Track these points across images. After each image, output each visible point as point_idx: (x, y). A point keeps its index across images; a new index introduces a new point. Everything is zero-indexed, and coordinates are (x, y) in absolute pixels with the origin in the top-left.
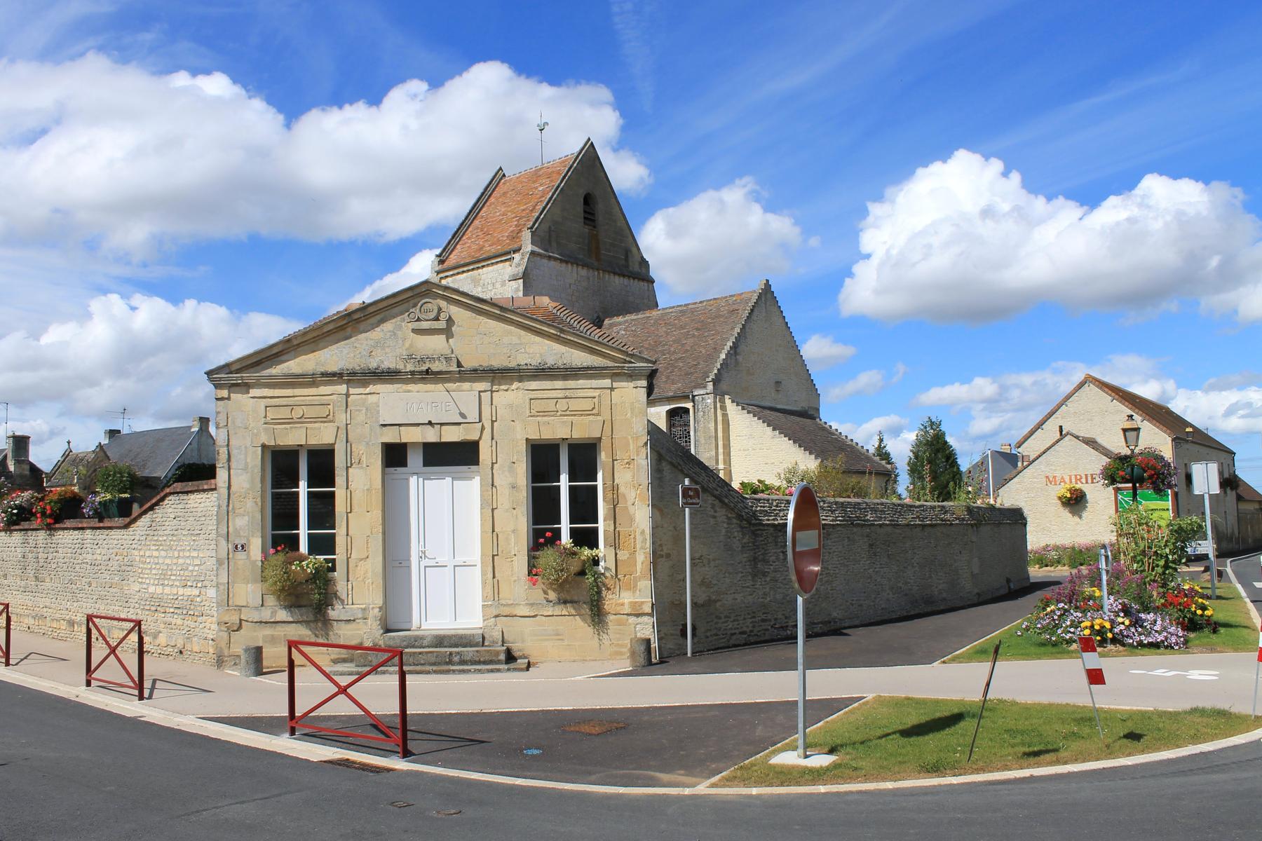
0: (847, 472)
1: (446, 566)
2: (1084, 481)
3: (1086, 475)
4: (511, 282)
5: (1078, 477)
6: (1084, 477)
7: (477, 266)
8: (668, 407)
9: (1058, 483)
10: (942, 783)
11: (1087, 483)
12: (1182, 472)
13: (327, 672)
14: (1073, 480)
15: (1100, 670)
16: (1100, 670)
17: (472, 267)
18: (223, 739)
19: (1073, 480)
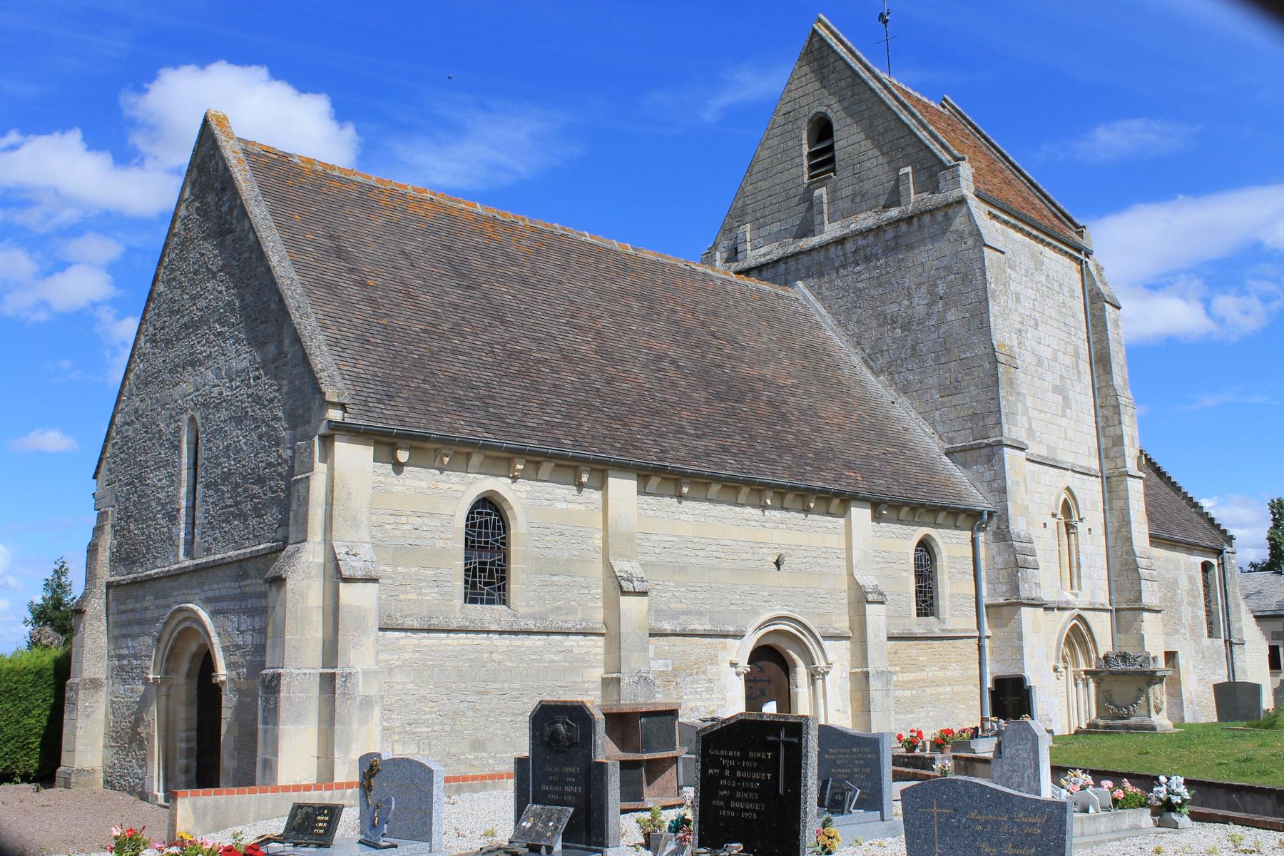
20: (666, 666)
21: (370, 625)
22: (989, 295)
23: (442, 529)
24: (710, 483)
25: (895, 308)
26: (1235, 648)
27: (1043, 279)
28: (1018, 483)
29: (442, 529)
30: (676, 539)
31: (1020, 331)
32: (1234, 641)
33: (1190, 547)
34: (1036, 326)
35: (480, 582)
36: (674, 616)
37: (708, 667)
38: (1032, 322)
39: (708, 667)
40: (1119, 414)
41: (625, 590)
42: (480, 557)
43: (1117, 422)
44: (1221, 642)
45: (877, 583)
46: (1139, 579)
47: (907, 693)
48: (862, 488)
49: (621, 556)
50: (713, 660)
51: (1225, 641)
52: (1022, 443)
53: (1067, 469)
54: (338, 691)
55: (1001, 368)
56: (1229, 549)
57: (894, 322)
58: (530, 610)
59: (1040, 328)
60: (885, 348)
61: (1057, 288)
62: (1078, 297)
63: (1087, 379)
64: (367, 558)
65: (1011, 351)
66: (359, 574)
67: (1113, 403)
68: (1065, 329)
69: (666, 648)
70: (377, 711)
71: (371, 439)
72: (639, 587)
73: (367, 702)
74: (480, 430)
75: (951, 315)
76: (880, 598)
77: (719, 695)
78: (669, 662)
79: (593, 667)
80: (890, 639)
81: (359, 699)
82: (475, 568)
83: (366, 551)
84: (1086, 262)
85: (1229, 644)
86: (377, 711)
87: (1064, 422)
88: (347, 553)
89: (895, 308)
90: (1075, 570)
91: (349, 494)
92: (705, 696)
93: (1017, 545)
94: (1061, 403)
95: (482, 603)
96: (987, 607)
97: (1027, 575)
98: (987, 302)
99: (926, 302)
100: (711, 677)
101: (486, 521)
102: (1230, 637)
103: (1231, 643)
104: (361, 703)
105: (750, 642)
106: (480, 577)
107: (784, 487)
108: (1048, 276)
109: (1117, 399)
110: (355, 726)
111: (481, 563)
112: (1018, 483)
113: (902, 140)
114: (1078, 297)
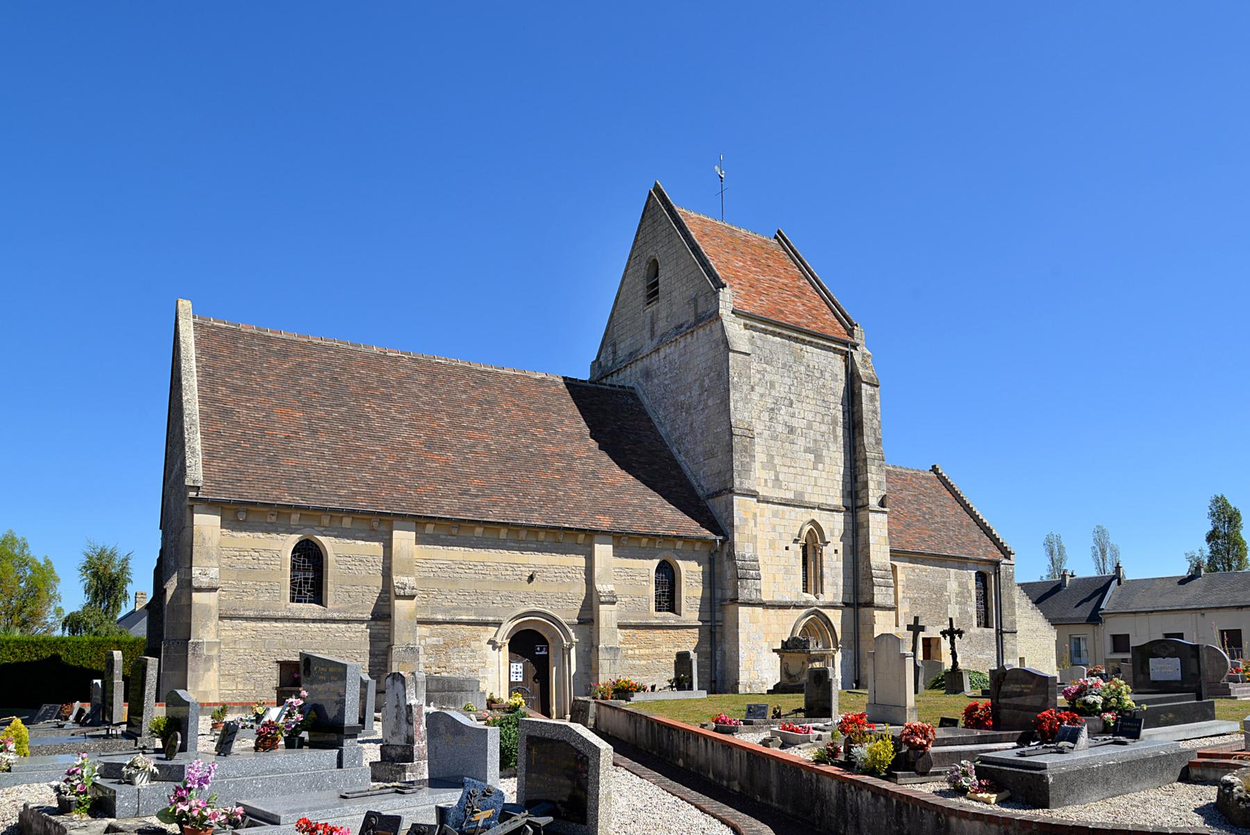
20: (439, 641)
21: (213, 615)
22: (731, 386)
23: (273, 559)
24: (475, 527)
25: (682, 398)
26: (1006, 636)
27: (802, 369)
28: (746, 520)
29: (273, 559)
30: (450, 562)
31: (772, 409)
32: (1004, 629)
33: (961, 562)
34: (791, 405)
35: (304, 590)
36: (447, 611)
37: (472, 643)
38: (787, 402)
39: (472, 643)
40: (866, 465)
41: (397, 594)
42: (305, 575)
43: (865, 472)
44: (993, 631)
45: (614, 590)
46: (873, 585)
47: (643, 662)
48: (605, 523)
49: (402, 573)
50: (477, 639)
51: (997, 630)
52: (755, 491)
53: (813, 508)
54: (190, 652)
55: (736, 439)
56: (1006, 561)
57: (682, 408)
58: (336, 607)
59: (794, 406)
60: (677, 426)
61: (818, 375)
62: (841, 380)
63: (841, 440)
64: (213, 577)
65: (749, 425)
66: (204, 586)
67: (863, 457)
68: (824, 405)
69: (440, 630)
70: (215, 665)
71: (218, 507)
72: (408, 592)
73: (209, 659)
74: (298, 498)
75: (710, 402)
76: (611, 599)
77: (479, 660)
78: (441, 639)
79: (381, 641)
80: (621, 626)
81: (204, 657)
82: (300, 582)
83: (214, 572)
84: (852, 353)
85: (1000, 633)
86: (215, 665)
87: (815, 473)
88: (200, 574)
89: (682, 398)
90: (819, 579)
91: (204, 539)
92: (468, 660)
93: (739, 563)
94: (813, 459)
95: (305, 602)
96: (993, 628)
97: (747, 584)
98: (729, 390)
99: (698, 393)
100: (474, 649)
101: (309, 553)
102: (1001, 627)
103: (1002, 632)
104: (205, 659)
105: (508, 627)
106: (304, 587)
107: (535, 526)
108: (809, 366)
109: (866, 455)
110: (201, 672)
111: (304, 579)
112: (746, 520)
113: (692, 274)
114: (841, 380)
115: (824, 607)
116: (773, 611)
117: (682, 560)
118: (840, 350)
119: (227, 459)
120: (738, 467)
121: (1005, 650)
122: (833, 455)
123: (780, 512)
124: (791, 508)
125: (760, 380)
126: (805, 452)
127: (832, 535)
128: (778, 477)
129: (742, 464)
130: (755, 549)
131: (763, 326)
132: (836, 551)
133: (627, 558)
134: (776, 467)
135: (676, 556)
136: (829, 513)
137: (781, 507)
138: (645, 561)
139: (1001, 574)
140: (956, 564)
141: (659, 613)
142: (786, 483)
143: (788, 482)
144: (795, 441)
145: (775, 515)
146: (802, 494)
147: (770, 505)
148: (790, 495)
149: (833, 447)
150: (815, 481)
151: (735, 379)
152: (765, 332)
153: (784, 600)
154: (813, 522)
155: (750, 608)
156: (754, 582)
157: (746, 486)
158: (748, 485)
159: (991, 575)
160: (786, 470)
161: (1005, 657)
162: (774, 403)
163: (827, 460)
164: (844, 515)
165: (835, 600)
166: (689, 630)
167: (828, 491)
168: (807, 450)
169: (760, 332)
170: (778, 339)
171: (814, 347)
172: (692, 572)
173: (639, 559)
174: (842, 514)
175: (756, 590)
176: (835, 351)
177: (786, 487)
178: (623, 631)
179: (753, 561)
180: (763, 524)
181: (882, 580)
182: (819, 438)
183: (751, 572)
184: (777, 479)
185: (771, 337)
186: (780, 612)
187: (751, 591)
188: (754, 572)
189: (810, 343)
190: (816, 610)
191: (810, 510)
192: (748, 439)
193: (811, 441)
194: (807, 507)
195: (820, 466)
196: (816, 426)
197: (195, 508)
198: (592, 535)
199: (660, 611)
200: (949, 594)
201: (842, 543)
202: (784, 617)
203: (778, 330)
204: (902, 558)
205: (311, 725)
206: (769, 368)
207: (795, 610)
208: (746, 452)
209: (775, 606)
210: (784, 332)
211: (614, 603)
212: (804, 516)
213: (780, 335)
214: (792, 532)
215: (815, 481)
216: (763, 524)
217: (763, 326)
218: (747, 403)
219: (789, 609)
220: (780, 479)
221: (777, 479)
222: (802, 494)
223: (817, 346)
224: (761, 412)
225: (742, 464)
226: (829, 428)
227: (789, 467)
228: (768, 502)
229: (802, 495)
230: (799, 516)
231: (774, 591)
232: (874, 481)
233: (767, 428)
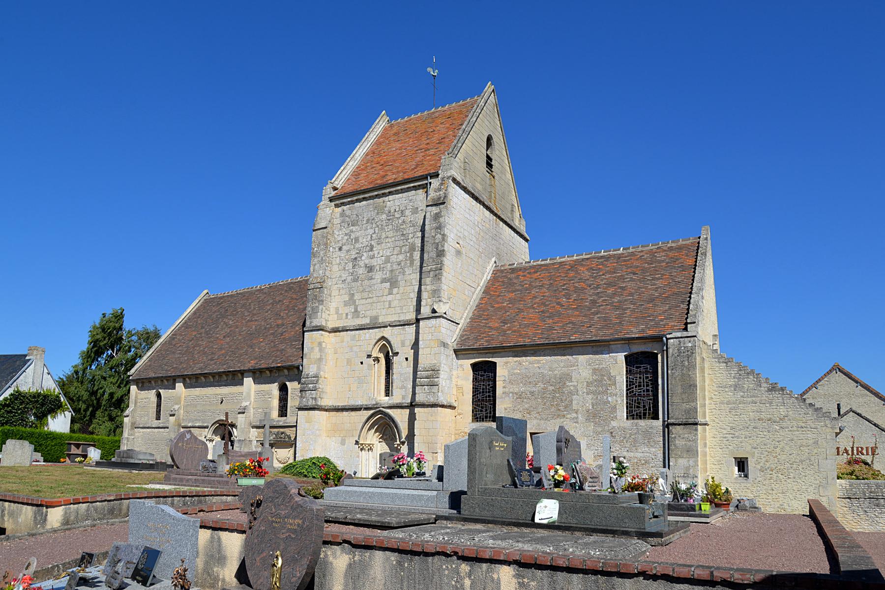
0: (849, 463)
1: (838, 405)
2: (865, 452)
3: (867, 448)
4: (429, 208)
5: (860, 449)
6: (865, 449)
7: (383, 192)
8: (473, 361)
9: (841, 453)
10: (659, 363)
11: (867, 454)
12: (208, 463)
13: (582, 456)
14: (855, 452)
15: (496, 363)
16: (496, 363)
17: (376, 193)
18: (84, 587)
19: (855, 452)
44: (659, 423)
51: (664, 421)
53: (386, 327)
87: (390, 297)
97: (306, 394)
115: (390, 407)
116: (347, 413)
117: (289, 381)
118: (419, 186)
119: (670, 324)
120: (309, 311)
121: (672, 447)
122: (407, 277)
123: (357, 336)
124: (366, 331)
125: (347, 240)
126: (382, 282)
127: (403, 345)
128: (357, 309)
129: (313, 309)
130: (319, 368)
131: (349, 199)
132: (407, 359)
133: (262, 384)
134: (355, 302)
135: (285, 379)
136: (400, 327)
137: (357, 332)
138: (271, 385)
139: (670, 351)
140: (590, 349)
141: (281, 418)
142: (364, 312)
143: (365, 311)
144: (374, 277)
145: (353, 338)
146: (376, 318)
147: (349, 332)
148: (366, 321)
149: (408, 271)
150: (390, 304)
151: (315, 249)
152: (352, 202)
153: (357, 404)
154: (383, 338)
155: (306, 412)
156: (311, 393)
157: (314, 324)
158: (316, 322)
159: (657, 354)
160: (364, 301)
161: (672, 455)
162: (357, 253)
163: (402, 283)
164: (416, 327)
165: (404, 401)
166: (291, 429)
167: (402, 309)
168: (384, 281)
169: (349, 204)
170: (364, 203)
171: (396, 194)
172: (295, 389)
173: (268, 384)
174: (414, 325)
175: (312, 398)
176: (415, 188)
177: (363, 315)
178: (258, 430)
179: (314, 377)
180: (343, 348)
181: (427, 379)
182: (395, 267)
183: (310, 385)
184: (356, 311)
185: (358, 203)
186: (353, 413)
187: (308, 400)
188: (312, 385)
189: (390, 193)
190: (380, 411)
191: (382, 329)
192: (318, 289)
193: (388, 273)
194: (380, 327)
195: (395, 290)
196: (393, 259)
197: (177, 380)
198: (243, 373)
199: (282, 416)
200: (575, 384)
201: (413, 351)
202: (356, 417)
203: (361, 196)
204: (503, 353)
205: (560, 485)
206: (354, 228)
207: (365, 411)
208: (316, 299)
209: (346, 409)
210: (366, 195)
211: (244, 413)
212: (377, 333)
213: (365, 199)
214: (366, 350)
215: (390, 304)
216: (343, 348)
217: (349, 199)
218: (322, 264)
219: (360, 410)
220: (359, 310)
221: (356, 311)
222: (376, 318)
223: (397, 192)
224: (346, 263)
225: (313, 309)
226: (406, 256)
227: (366, 298)
228: (347, 330)
229: (376, 318)
230: (372, 336)
231: (349, 398)
232: (428, 292)
233: (350, 274)
